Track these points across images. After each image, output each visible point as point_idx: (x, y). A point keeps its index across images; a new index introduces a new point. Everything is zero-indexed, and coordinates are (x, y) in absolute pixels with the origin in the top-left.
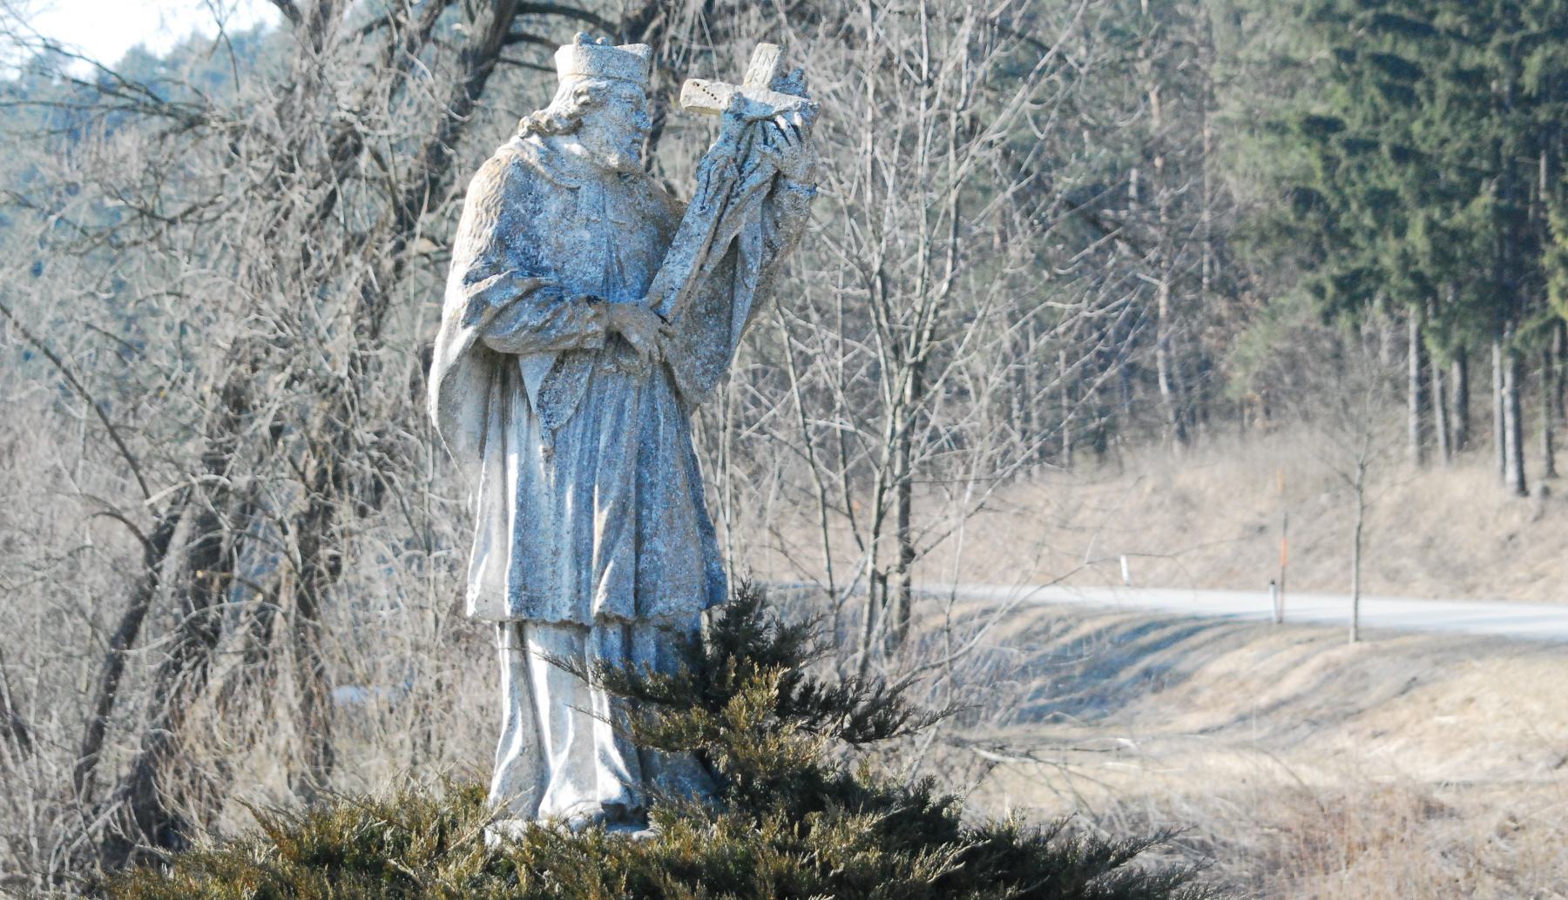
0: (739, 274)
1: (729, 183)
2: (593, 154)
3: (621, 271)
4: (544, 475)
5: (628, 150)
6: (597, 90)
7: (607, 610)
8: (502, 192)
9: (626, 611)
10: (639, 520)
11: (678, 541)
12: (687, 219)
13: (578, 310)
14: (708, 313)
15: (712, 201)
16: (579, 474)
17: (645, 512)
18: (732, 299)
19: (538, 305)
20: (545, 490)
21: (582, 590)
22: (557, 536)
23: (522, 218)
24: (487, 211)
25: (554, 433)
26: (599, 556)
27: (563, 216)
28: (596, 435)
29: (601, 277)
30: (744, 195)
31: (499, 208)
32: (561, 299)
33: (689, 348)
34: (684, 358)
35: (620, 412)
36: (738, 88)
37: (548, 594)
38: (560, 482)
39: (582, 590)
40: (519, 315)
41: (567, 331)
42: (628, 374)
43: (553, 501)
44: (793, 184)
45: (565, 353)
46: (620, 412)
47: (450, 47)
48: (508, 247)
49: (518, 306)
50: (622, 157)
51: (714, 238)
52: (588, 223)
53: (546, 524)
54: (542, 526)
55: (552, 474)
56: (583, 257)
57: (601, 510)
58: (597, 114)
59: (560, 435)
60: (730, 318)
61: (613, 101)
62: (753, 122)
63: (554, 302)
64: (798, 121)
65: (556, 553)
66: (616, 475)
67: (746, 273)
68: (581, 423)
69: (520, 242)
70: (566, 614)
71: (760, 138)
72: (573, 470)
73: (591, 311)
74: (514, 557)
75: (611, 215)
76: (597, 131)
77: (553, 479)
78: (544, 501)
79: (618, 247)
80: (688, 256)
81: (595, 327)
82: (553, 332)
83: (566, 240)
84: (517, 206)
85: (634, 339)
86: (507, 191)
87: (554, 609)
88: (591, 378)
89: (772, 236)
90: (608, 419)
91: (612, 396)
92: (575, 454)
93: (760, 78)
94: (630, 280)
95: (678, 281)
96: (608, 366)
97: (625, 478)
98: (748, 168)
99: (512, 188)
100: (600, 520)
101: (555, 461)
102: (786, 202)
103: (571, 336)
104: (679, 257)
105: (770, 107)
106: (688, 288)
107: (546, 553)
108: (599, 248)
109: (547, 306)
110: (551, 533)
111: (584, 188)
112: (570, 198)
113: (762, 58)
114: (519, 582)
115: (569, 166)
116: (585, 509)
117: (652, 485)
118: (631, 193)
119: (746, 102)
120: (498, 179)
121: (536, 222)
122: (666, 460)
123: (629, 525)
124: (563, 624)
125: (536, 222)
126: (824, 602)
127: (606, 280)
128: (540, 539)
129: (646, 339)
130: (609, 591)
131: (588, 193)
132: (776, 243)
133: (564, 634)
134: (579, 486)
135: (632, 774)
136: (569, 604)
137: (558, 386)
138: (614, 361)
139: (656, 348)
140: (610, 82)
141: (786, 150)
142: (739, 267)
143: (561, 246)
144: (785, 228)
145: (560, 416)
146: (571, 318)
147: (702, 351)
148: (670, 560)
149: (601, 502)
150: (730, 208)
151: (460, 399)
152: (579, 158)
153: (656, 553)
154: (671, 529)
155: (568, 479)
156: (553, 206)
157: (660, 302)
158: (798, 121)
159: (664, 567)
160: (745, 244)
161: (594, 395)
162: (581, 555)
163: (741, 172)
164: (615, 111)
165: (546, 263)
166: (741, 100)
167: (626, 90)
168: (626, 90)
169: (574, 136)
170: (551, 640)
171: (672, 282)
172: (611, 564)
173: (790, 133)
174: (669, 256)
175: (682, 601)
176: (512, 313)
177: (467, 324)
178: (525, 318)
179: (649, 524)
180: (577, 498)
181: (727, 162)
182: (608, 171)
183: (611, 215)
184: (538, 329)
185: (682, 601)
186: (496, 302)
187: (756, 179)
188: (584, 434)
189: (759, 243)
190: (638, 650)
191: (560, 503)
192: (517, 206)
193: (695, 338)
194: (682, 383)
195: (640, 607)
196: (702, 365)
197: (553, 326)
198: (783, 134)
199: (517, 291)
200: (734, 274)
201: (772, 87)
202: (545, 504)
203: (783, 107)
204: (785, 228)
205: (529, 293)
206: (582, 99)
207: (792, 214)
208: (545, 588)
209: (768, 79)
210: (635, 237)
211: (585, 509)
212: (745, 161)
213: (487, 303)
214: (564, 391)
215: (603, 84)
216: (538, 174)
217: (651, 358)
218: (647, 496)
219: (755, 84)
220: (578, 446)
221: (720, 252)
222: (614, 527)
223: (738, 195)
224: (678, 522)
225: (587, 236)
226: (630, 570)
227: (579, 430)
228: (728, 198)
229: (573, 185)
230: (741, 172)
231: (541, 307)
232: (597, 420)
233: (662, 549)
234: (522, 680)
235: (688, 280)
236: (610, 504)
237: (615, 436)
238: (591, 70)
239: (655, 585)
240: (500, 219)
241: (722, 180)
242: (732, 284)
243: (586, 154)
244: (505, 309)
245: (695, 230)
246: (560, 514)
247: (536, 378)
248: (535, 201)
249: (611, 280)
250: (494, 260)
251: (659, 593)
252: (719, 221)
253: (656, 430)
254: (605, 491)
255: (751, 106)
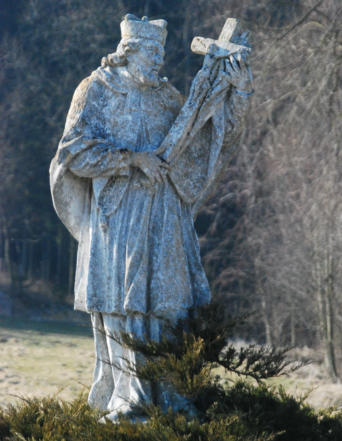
0: (213, 138)
1: (205, 91)
2: (133, 76)
3: (148, 135)
4: (104, 239)
5: (149, 74)
6: (134, 44)
7: (130, 307)
8: (86, 96)
9: (141, 308)
10: (150, 263)
11: (170, 273)
12: (183, 109)
13: (114, 156)
14: (199, 157)
15: (196, 100)
16: (120, 239)
17: (155, 258)
18: (209, 149)
19: (94, 153)
20: (104, 247)
21: (120, 297)
22: (110, 270)
23: (97, 110)
24: (79, 105)
25: (108, 218)
26: (127, 280)
27: (118, 107)
28: (128, 221)
29: (136, 139)
30: (212, 97)
31: (84, 104)
32: (106, 150)
33: (187, 175)
34: (183, 180)
35: (141, 206)
36: (216, 42)
37: (107, 299)
38: (111, 242)
39: (120, 297)
40: (85, 158)
41: (109, 166)
42: (147, 188)
43: (108, 252)
44: (239, 91)
45: (112, 177)
46: (141, 206)
47: (328, 18)
48: (87, 124)
49: (84, 154)
50: (145, 78)
51: (196, 119)
52: (131, 112)
53: (105, 264)
54: (103, 265)
55: (107, 238)
56: (127, 129)
57: (129, 257)
58: (134, 56)
59: (111, 219)
60: (208, 160)
61: (142, 49)
62: (219, 59)
63: (103, 152)
64: (239, 58)
65: (109, 278)
66: (137, 240)
67: (217, 137)
68: (122, 213)
69: (94, 121)
70: (113, 309)
71: (222, 68)
72: (117, 236)
73: (121, 157)
74: (89, 279)
75: (143, 107)
76: (134, 65)
77: (107, 240)
78: (104, 252)
79: (146, 124)
80: (181, 128)
81: (123, 164)
82: (102, 167)
83: (119, 120)
84: (93, 103)
85: (146, 170)
86: (89, 95)
87: (109, 307)
88: (128, 191)
89: (230, 117)
90: (134, 212)
91: (138, 199)
92: (118, 228)
93: (226, 36)
94: (152, 140)
95: (174, 141)
96: (136, 184)
97: (142, 241)
98: (216, 82)
99: (91, 94)
100: (128, 261)
101: (108, 232)
102: (235, 100)
103: (113, 169)
104: (177, 129)
105: (229, 51)
106: (180, 144)
107: (105, 280)
108: (136, 124)
109: (99, 154)
110: (107, 268)
111: (129, 94)
112: (123, 99)
113: (228, 26)
114: (92, 292)
115: (123, 82)
116: (121, 257)
117: (159, 244)
118: (158, 96)
119: (218, 49)
120: (85, 89)
121: (104, 111)
122: (168, 232)
123: (144, 265)
124: (114, 315)
125: (104, 111)
126: (254, 308)
127: (139, 141)
128: (103, 271)
129: (152, 171)
130: (130, 298)
131: (132, 96)
132: (233, 121)
133: (116, 319)
134: (119, 245)
135: (145, 391)
136: (114, 304)
137: (111, 194)
138: (139, 181)
139: (158, 175)
140: (141, 40)
141: (232, 73)
142: (213, 134)
143: (117, 123)
144: (236, 113)
145: (110, 209)
146: (111, 160)
147: (194, 177)
148: (166, 283)
149: (129, 253)
150: (205, 103)
151: (68, 200)
152: (127, 78)
153: (159, 279)
154: (167, 267)
155: (114, 241)
156: (113, 103)
157: (164, 152)
158: (239, 58)
159: (163, 286)
160: (216, 122)
161: (129, 199)
162: (120, 280)
163: (211, 85)
164: (143, 54)
165: (108, 132)
166: (215, 48)
167: (149, 44)
168: (149, 44)
169: (125, 67)
170: (110, 322)
171: (171, 141)
172: (132, 285)
173: (235, 64)
174: (172, 128)
175: (171, 304)
176: (82, 157)
177: (59, 164)
178: (88, 160)
179: (156, 264)
180: (118, 252)
181: (204, 80)
182: (141, 85)
183: (143, 107)
184: (95, 166)
185: (171, 304)
186: (73, 152)
187: (218, 88)
188: (123, 219)
189: (223, 121)
190: (152, 328)
191: (111, 253)
192: (93, 103)
193: (191, 169)
194: (181, 193)
195: (149, 306)
196: (194, 183)
197: (102, 164)
198: (231, 66)
199: (83, 146)
200: (211, 138)
201: (231, 41)
202: (104, 254)
203: (233, 51)
204: (236, 113)
205: (90, 147)
206: (127, 48)
207: (238, 106)
208: (105, 296)
209: (230, 37)
210: (158, 118)
211: (121, 257)
212: (215, 79)
213: (69, 152)
214: (113, 197)
215: (137, 41)
216: (106, 87)
217: (156, 181)
218: (156, 250)
219: (224, 39)
220: (120, 224)
221: (198, 126)
222: (134, 266)
223: (209, 97)
224: (171, 264)
225: (130, 118)
226: (143, 287)
227: (121, 217)
228: (204, 98)
229: (124, 92)
230: (211, 85)
231: (95, 154)
232: (130, 212)
233: (162, 277)
234: (102, 342)
235: (179, 140)
236: (133, 254)
237: (138, 220)
238: (132, 33)
239: (157, 295)
240: (84, 109)
241: (201, 88)
242: (210, 142)
243: (130, 76)
244: (77, 155)
245: (186, 115)
246: (111, 259)
247: (98, 191)
248: (104, 100)
249: (142, 140)
250: (79, 130)
251: (159, 300)
252: (199, 109)
253: (162, 217)
254: (131, 248)
255: (221, 51)
